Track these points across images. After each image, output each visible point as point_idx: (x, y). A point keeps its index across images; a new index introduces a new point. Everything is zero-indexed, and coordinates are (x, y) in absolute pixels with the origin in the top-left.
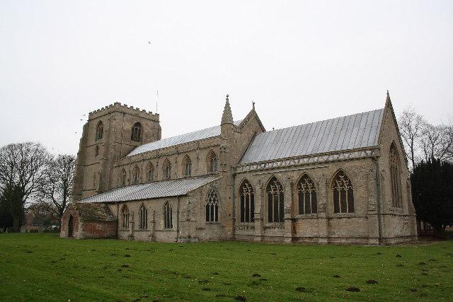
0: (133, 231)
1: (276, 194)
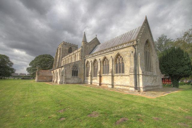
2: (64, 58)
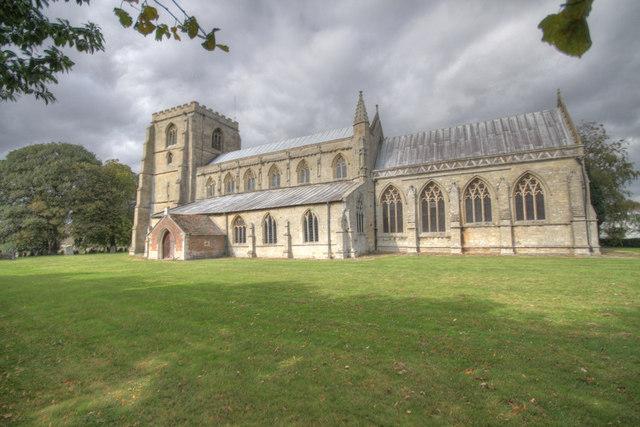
0: (254, 247)
1: (433, 201)
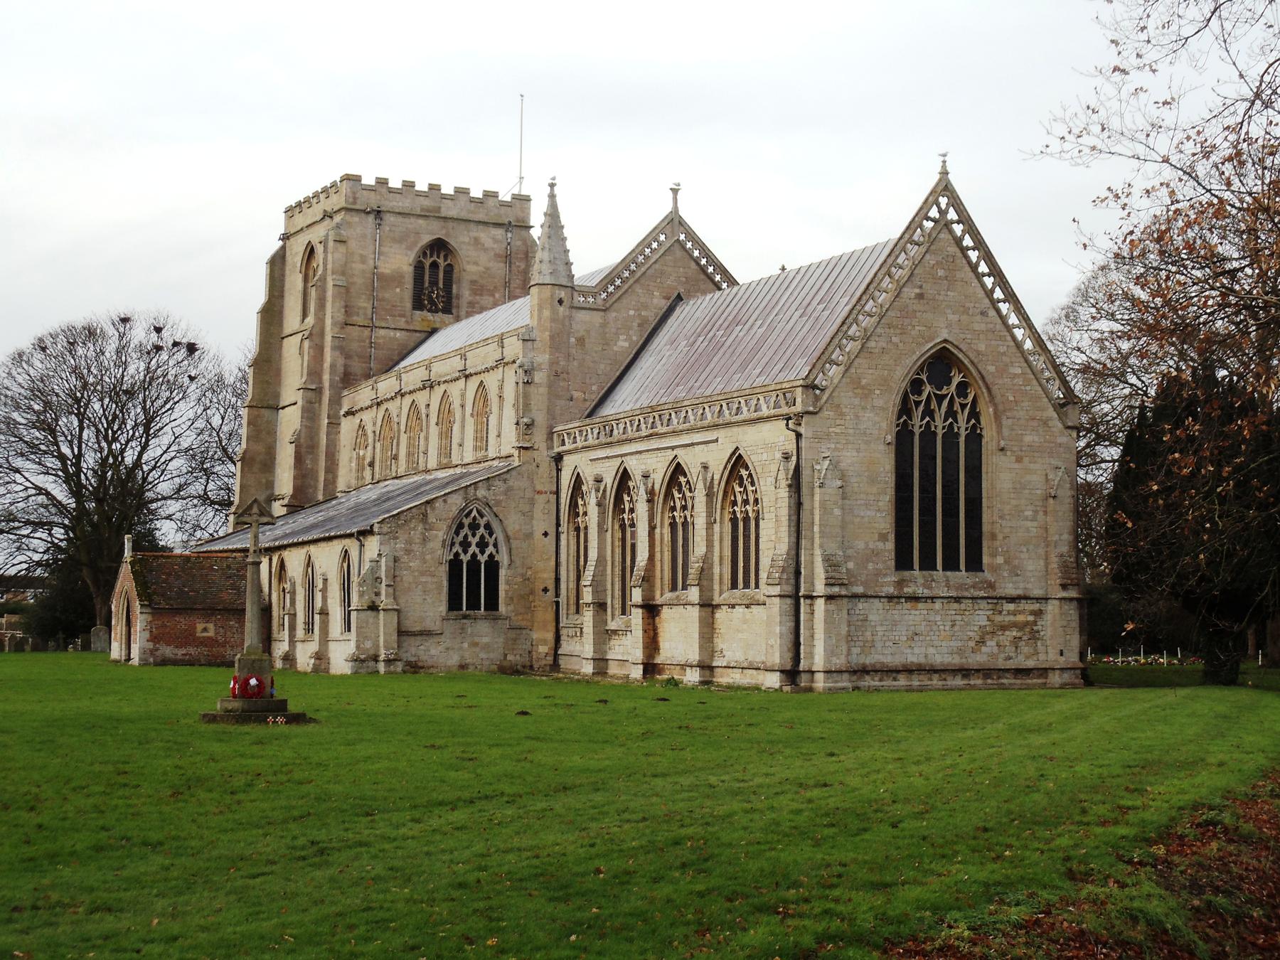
0: (292, 642)
2: (364, 395)
